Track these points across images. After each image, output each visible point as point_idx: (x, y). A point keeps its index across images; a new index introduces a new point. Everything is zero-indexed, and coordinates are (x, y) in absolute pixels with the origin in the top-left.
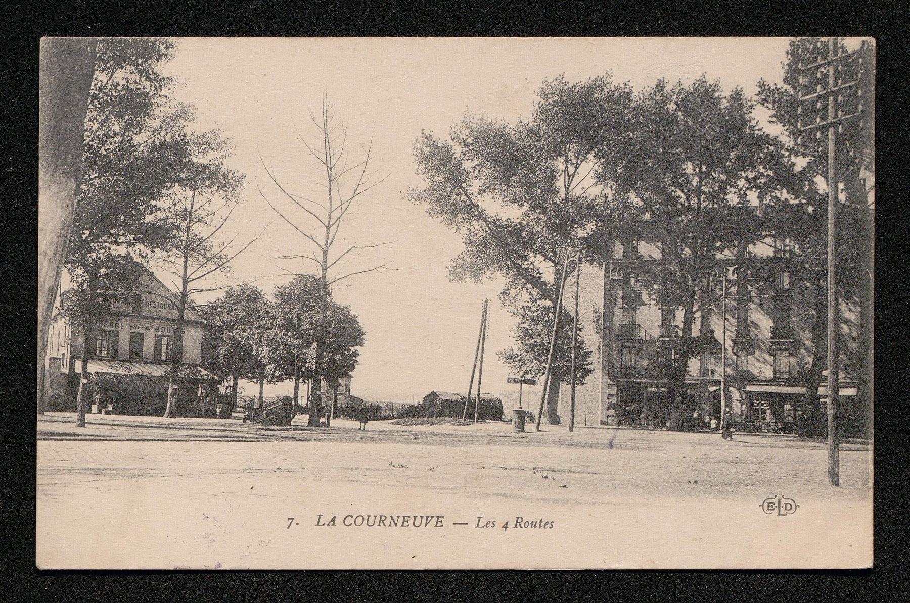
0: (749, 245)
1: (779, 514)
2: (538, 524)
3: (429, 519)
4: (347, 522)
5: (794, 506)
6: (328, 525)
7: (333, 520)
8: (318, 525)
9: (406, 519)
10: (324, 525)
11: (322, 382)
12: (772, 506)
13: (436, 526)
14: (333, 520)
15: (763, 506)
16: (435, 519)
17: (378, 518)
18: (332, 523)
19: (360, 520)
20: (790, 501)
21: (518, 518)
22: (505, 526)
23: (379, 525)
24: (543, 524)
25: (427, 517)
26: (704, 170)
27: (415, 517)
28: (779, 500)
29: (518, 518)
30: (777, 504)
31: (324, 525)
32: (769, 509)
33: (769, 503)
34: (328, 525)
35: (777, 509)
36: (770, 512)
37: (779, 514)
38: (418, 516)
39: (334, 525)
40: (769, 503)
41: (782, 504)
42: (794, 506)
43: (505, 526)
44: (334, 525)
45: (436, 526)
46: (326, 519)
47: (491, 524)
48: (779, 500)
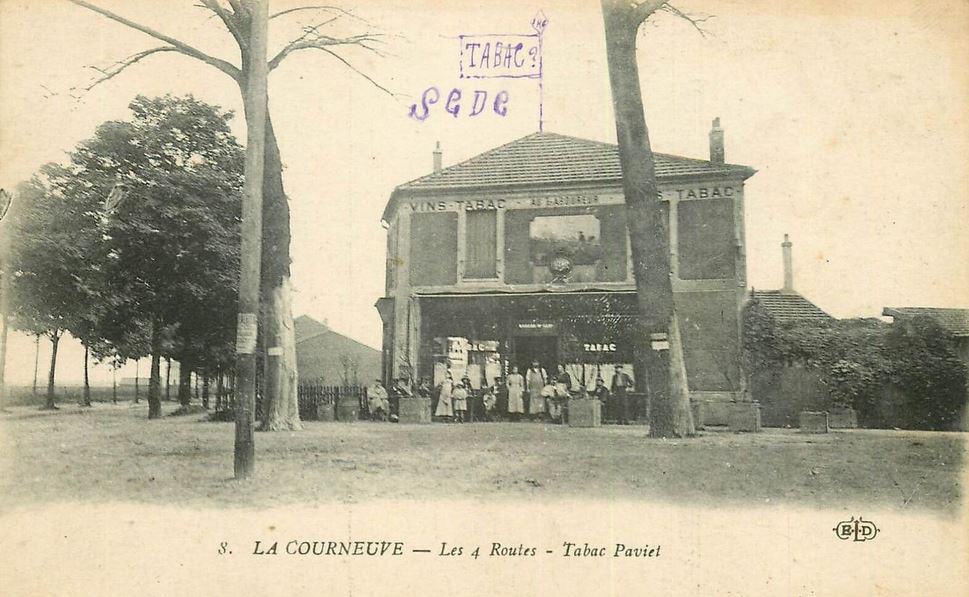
0: (654, 348)
1: (856, 539)
2: (517, 552)
3: (386, 545)
4: (291, 550)
5: (873, 531)
6: (268, 553)
7: (274, 547)
8: (255, 553)
9: (360, 545)
10: (262, 553)
11: (256, 298)
12: (848, 530)
13: (395, 553)
14: (274, 547)
15: (837, 529)
16: (393, 546)
17: (327, 545)
18: (272, 551)
19: (304, 548)
20: (867, 524)
21: (494, 544)
22: (476, 553)
23: (328, 553)
24: (523, 551)
25: (384, 543)
26: (537, 364)
27: (370, 543)
28: (857, 522)
29: (494, 544)
30: (853, 528)
31: (262, 553)
32: (844, 534)
33: (844, 527)
34: (268, 553)
35: (853, 534)
36: (845, 536)
37: (856, 539)
38: (522, 556)
39: (274, 553)
40: (844, 527)
41: (860, 528)
42: (873, 531)
43: (476, 553)
44: (274, 553)
45: (395, 553)
46: (265, 546)
47: (458, 552)
48: (857, 522)
